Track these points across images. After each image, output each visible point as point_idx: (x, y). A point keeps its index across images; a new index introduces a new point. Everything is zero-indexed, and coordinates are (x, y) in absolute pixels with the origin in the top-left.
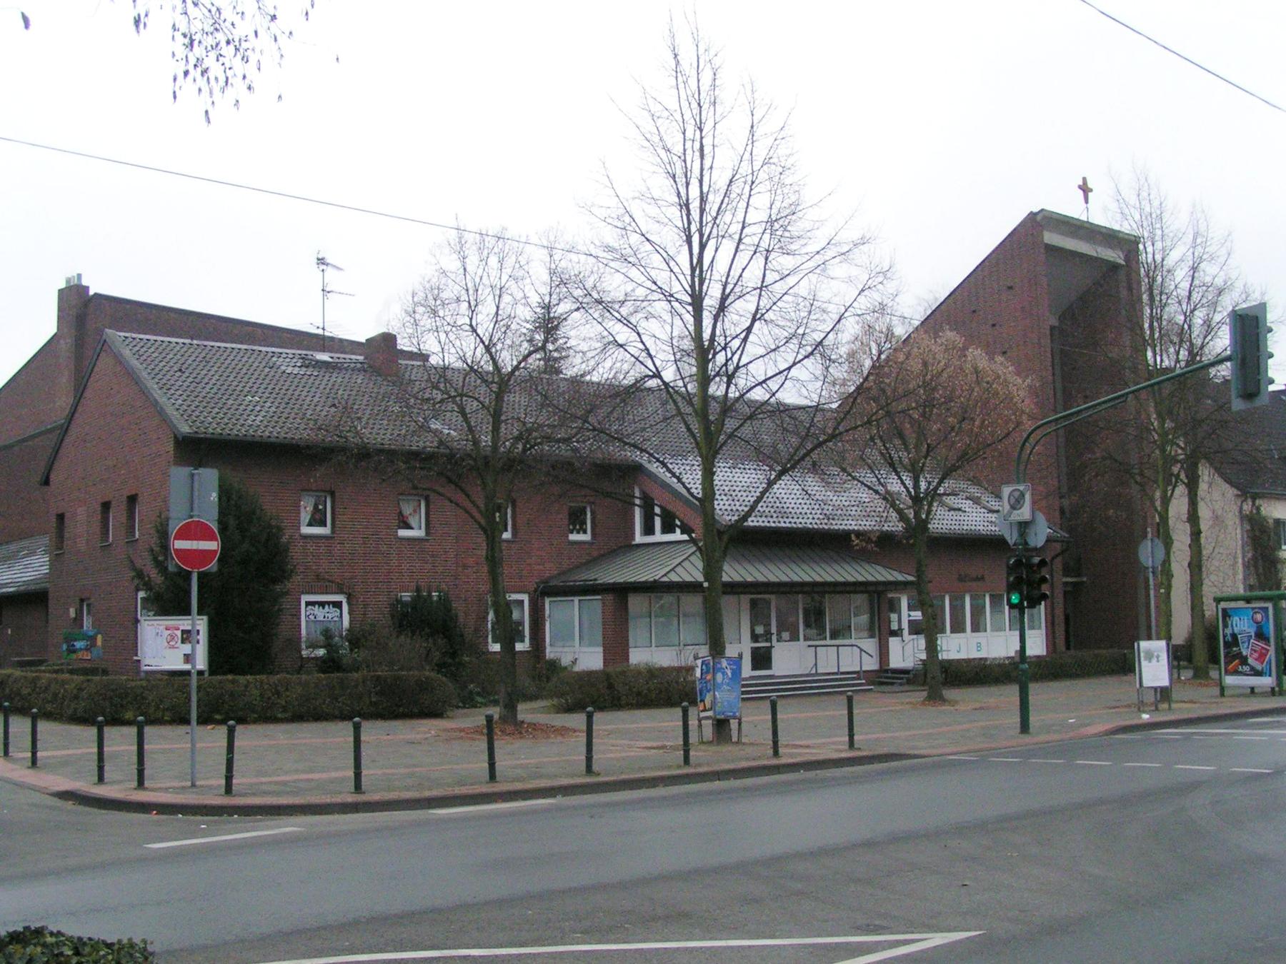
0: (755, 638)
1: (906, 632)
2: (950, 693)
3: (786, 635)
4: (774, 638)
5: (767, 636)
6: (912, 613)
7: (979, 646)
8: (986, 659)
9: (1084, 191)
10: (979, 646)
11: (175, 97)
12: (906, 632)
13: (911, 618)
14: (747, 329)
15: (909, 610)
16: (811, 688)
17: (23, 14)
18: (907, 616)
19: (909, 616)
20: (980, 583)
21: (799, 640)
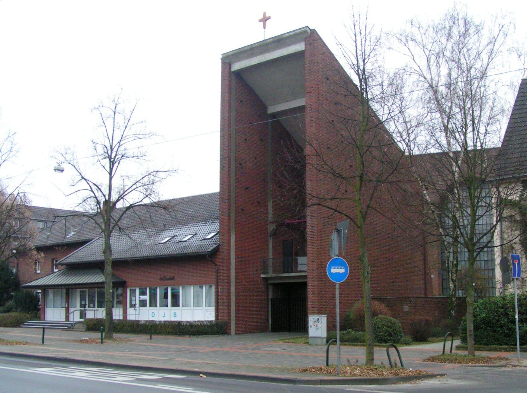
0: (81, 306)
1: (137, 306)
2: (115, 335)
3: (92, 305)
4: (87, 306)
5: (85, 306)
6: (141, 297)
7: (175, 315)
8: (139, 321)
9: (266, 20)
10: (175, 315)
11: (368, 6)
12: (137, 306)
13: (140, 299)
14: (112, 177)
15: (139, 295)
16: (36, 325)
17: (264, 28)
18: (138, 298)
19: (140, 298)
20: (172, 281)
21: (156, 306)
